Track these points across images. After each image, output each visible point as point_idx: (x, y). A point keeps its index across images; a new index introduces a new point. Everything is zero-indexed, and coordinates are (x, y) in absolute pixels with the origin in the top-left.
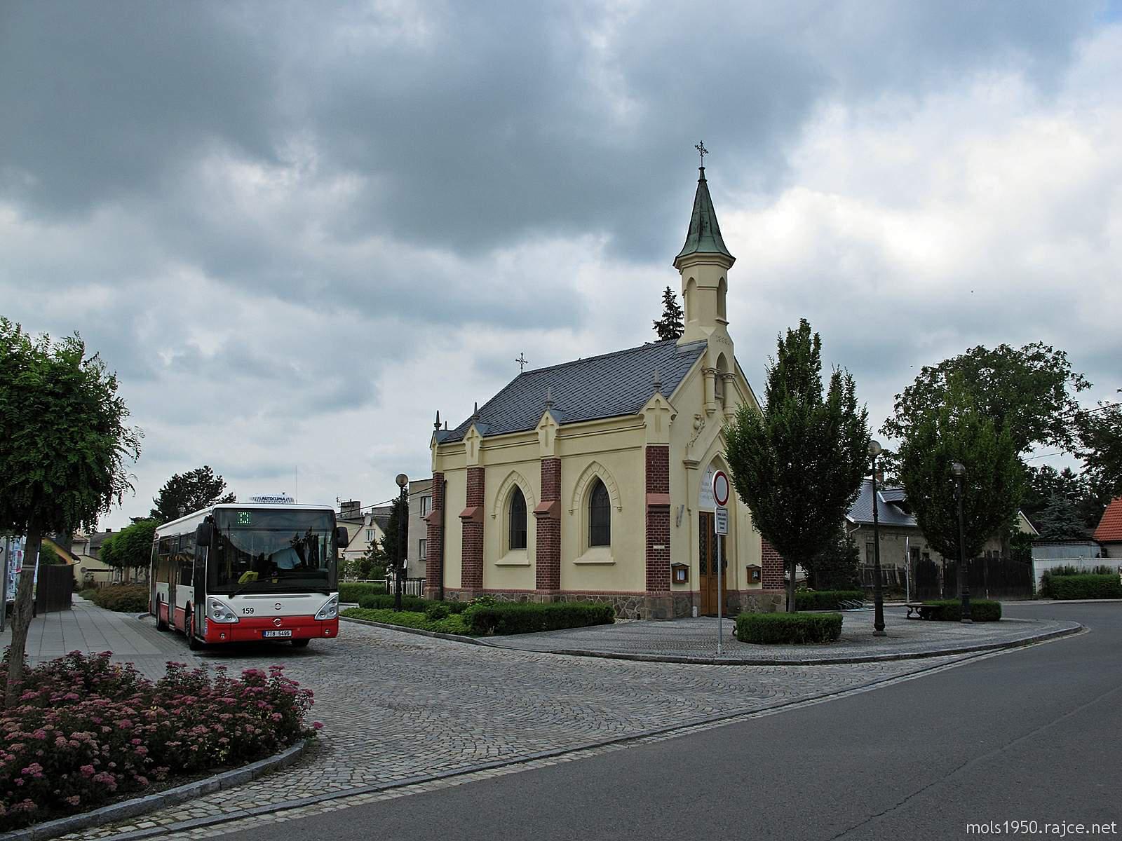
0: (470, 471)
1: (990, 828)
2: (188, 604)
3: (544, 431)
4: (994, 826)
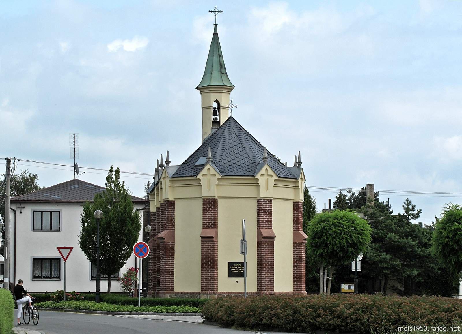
1: (408, 328)
3: (205, 177)
4: (409, 328)
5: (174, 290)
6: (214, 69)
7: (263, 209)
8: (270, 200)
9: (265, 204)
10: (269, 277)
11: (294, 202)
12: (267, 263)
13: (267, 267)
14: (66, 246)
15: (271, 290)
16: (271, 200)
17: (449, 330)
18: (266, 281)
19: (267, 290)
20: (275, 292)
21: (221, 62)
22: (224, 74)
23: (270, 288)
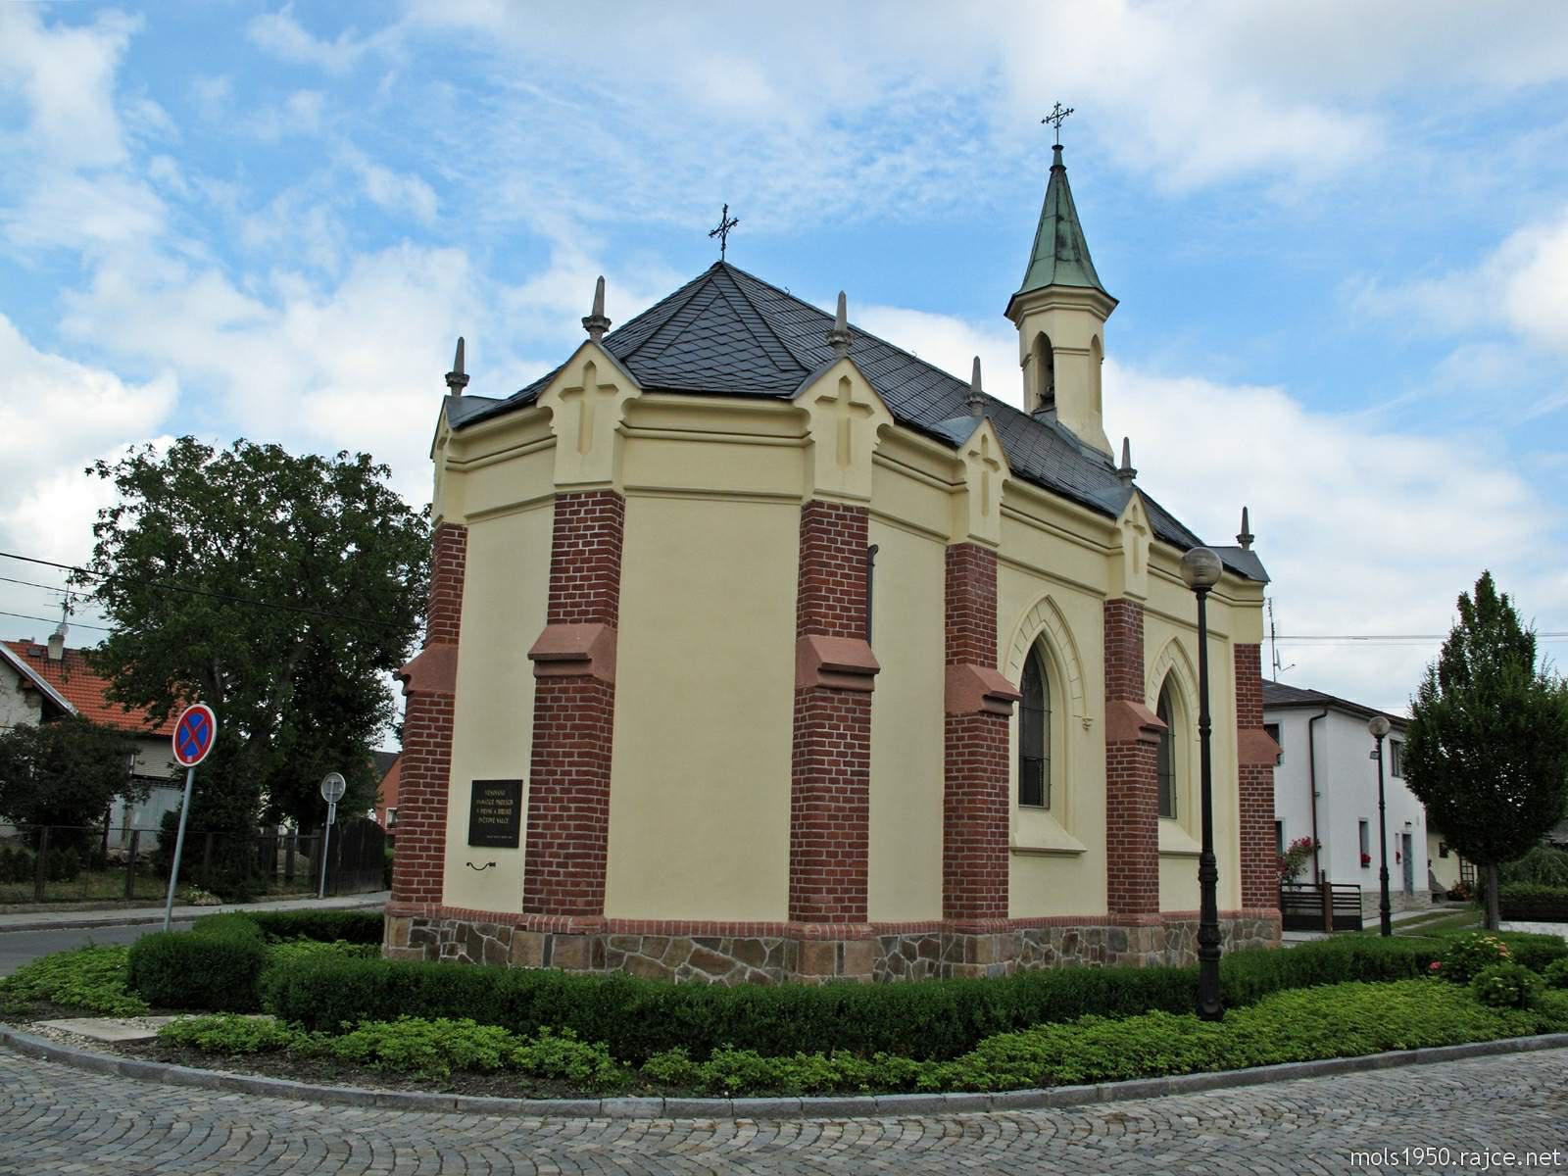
0: (564, 503)
3: (574, 403)
4: (1389, 1155)
6: (1040, 254)
9: (578, 512)
10: (561, 846)
12: (555, 782)
13: (555, 800)
15: (852, 919)
17: (1524, 1163)
18: (544, 864)
19: (550, 912)
23: (562, 903)
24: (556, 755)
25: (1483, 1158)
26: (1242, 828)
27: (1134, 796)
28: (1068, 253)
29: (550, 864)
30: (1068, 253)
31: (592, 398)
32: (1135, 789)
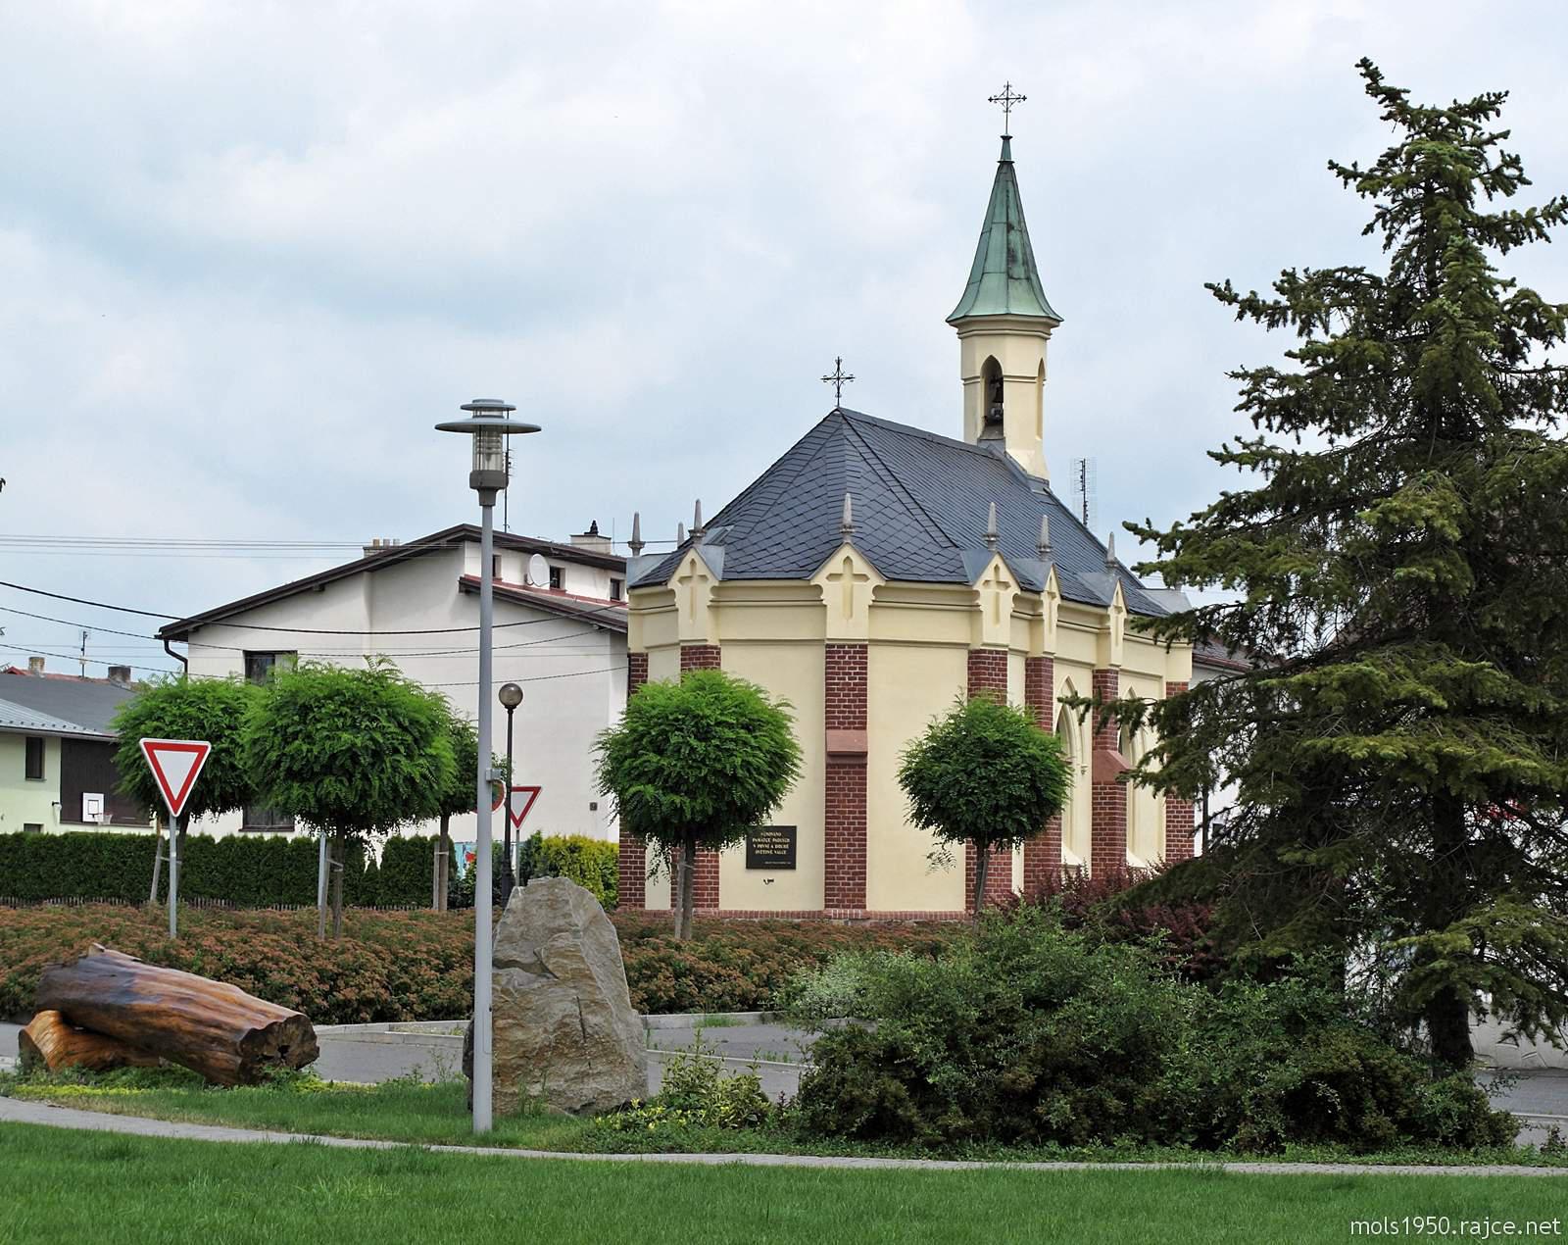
2: (1224, 785)
3: (834, 583)
4: (1388, 1224)
5: (642, 906)
6: (990, 267)
7: (838, 674)
8: (861, 646)
10: (850, 868)
11: (970, 652)
13: (844, 840)
14: (522, 785)
16: (866, 646)
18: (839, 879)
19: (844, 907)
20: (867, 913)
21: (1012, 246)
22: (1017, 283)
24: (844, 812)
25: (1483, 1227)
26: (1168, 846)
27: (1115, 824)
28: (1019, 271)
29: (843, 878)
30: (1019, 271)
31: (846, 581)
32: (1115, 819)
